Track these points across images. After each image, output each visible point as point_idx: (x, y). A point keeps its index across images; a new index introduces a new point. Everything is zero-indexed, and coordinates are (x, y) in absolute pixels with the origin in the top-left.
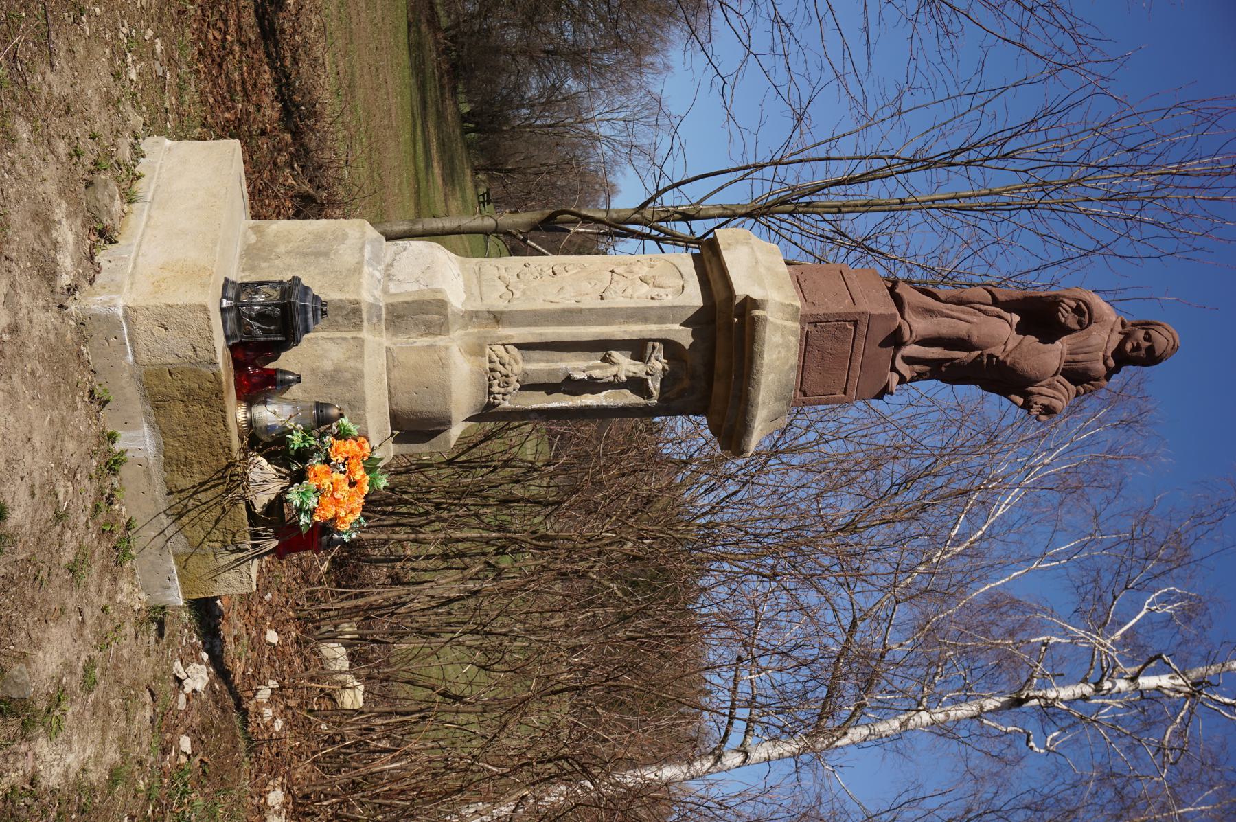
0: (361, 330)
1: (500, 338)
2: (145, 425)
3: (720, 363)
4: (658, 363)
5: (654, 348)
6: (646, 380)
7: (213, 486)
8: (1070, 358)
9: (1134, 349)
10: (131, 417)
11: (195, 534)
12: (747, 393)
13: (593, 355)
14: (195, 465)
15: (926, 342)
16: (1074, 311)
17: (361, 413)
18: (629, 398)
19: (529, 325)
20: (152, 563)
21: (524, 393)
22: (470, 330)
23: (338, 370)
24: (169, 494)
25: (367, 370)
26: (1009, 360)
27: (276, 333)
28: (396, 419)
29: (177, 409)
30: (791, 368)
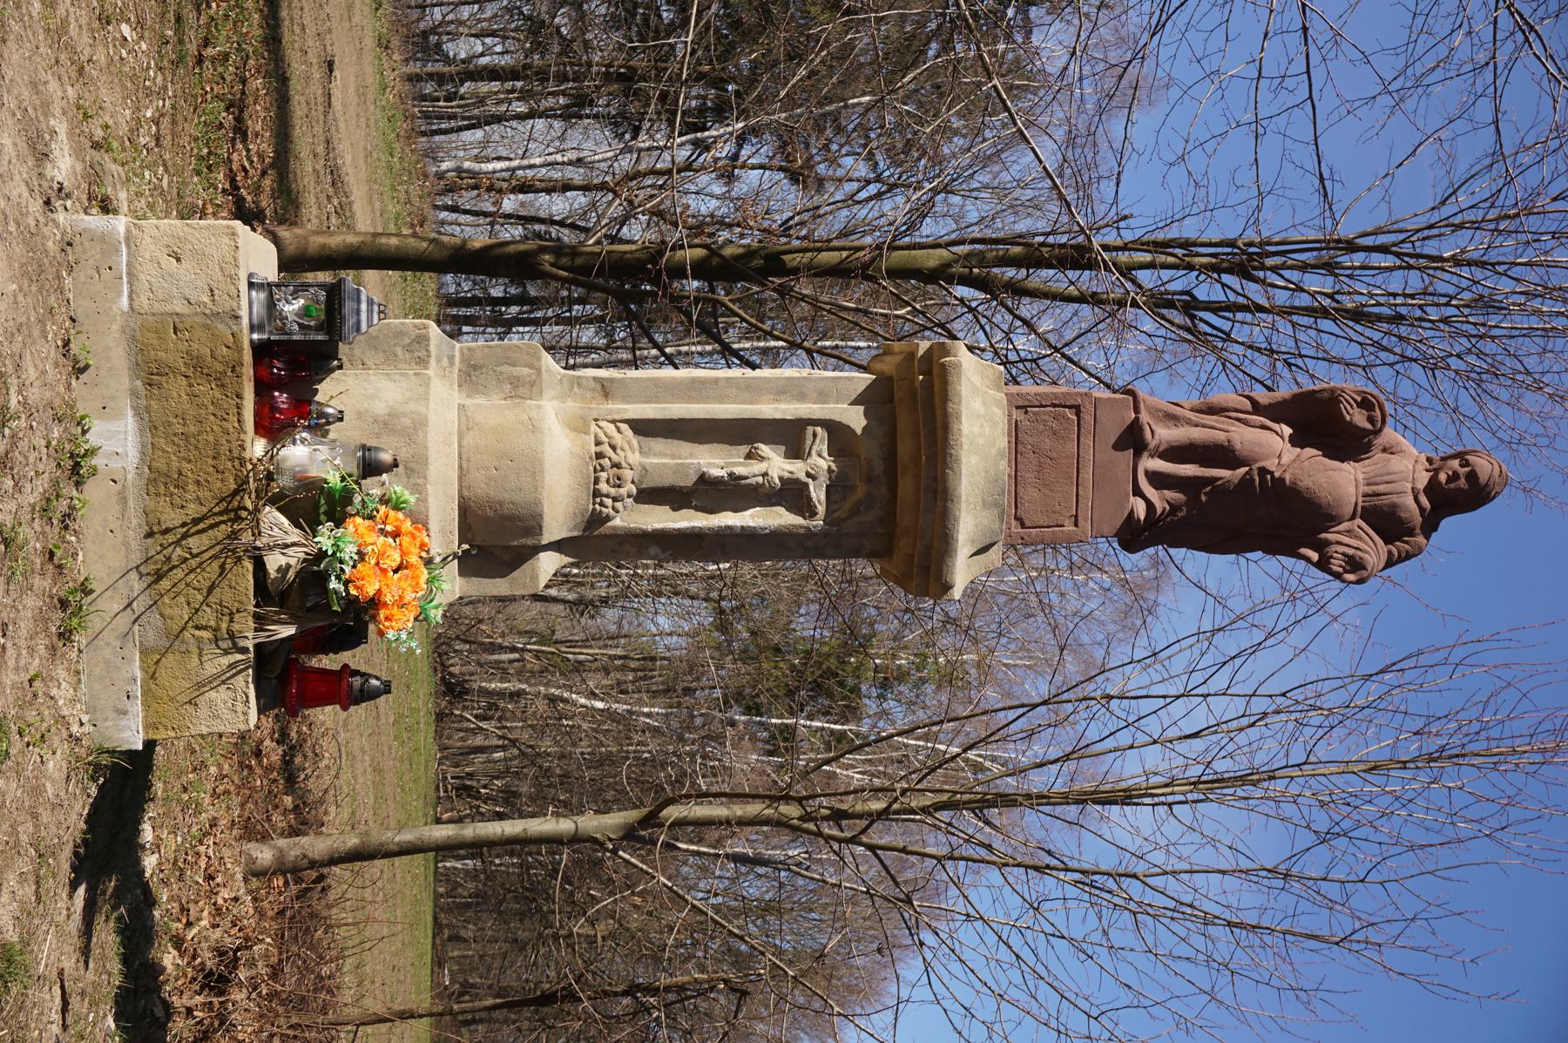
0: (426, 368)
1: (610, 412)
2: (130, 413)
3: (904, 447)
4: (820, 461)
5: (815, 435)
6: (807, 485)
7: (212, 527)
8: (1369, 490)
9: (1450, 479)
10: (113, 398)
11: (176, 612)
12: (945, 480)
13: (734, 449)
14: (191, 487)
15: (1175, 453)
16: (1360, 405)
17: (420, 481)
18: (777, 518)
19: (648, 400)
20: (107, 662)
21: (642, 507)
22: (570, 403)
23: (393, 415)
24: (150, 534)
25: (433, 418)
26: (1288, 477)
27: (318, 329)
28: (470, 517)
29: (177, 388)
30: (1000, 453)
